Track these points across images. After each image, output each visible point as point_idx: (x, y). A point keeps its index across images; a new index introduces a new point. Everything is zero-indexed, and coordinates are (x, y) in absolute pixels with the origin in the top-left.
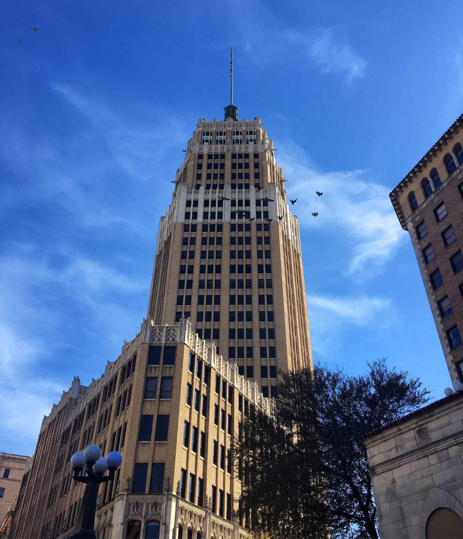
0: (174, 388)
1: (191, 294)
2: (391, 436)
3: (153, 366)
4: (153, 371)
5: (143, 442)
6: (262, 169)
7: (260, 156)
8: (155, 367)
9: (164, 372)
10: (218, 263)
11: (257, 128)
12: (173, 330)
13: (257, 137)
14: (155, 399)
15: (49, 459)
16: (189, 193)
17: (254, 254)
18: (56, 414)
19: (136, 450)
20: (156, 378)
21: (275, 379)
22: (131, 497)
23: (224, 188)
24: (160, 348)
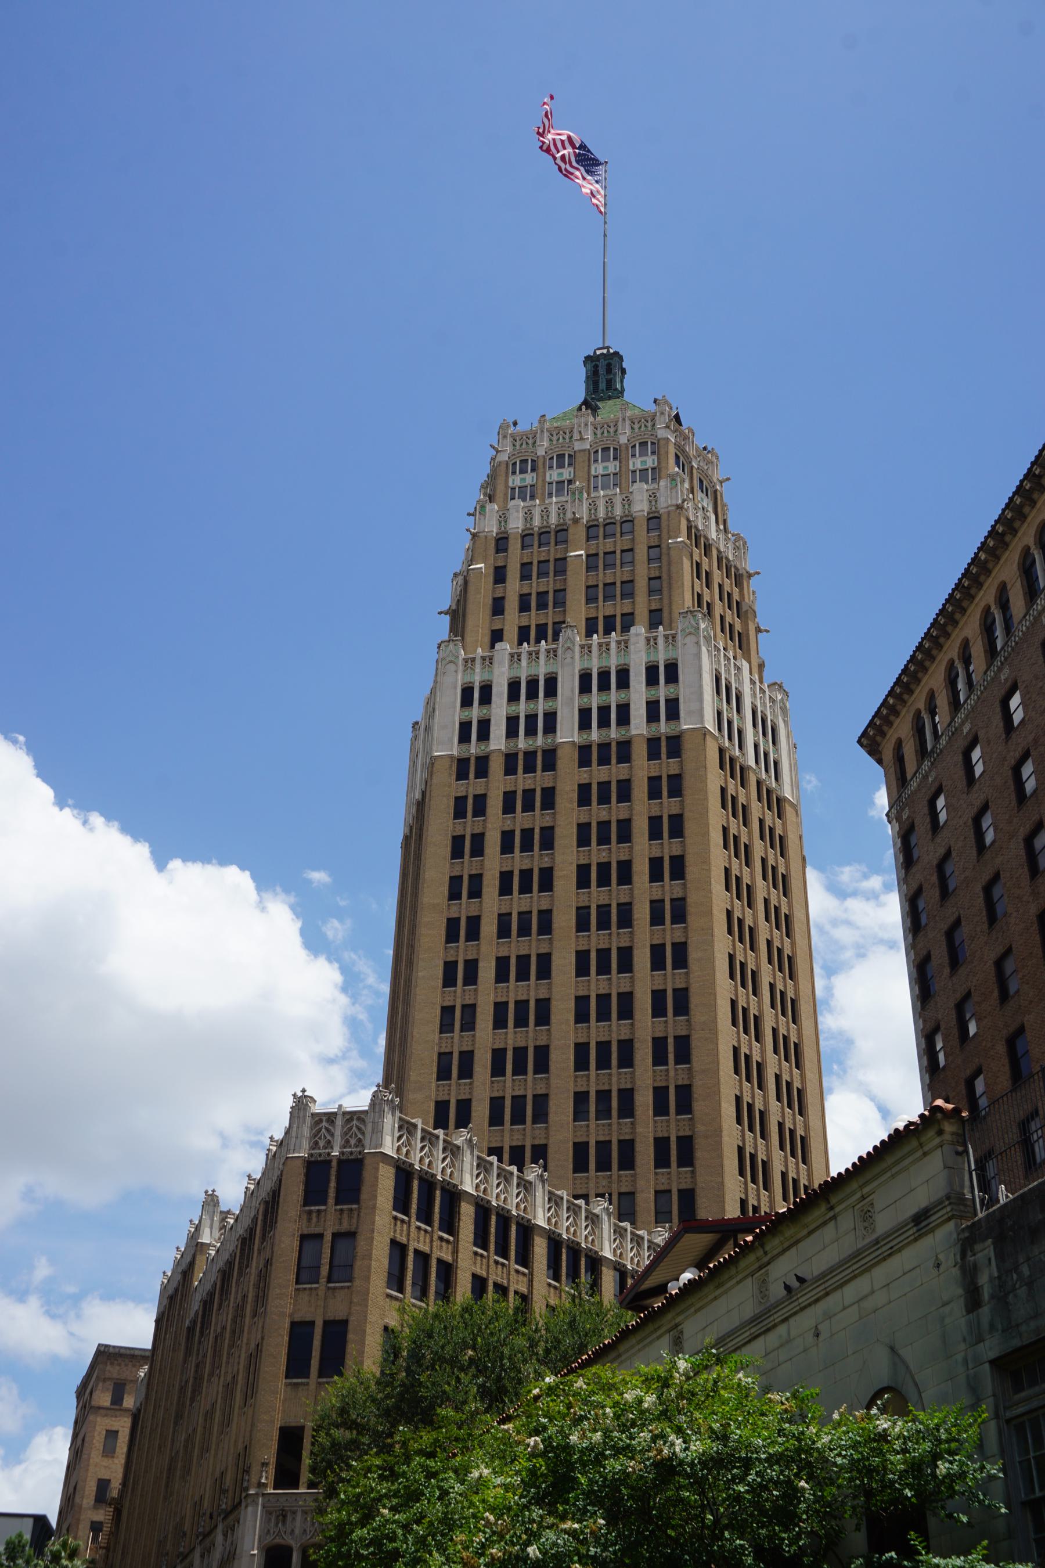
4: (314, 1219)
6: (669, 564)
8: (319, 1211)
20: (320, 1236)
24: (327, 1163)
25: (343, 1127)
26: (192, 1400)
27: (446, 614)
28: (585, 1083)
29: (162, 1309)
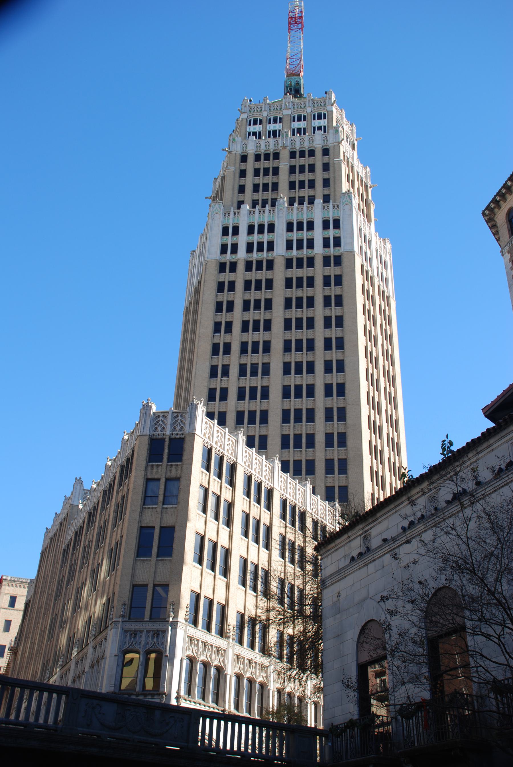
0: (182, 491)
1: (229, 361)
2: (342, 544)
3: (154, 464)
5: (142, 559)
6: (334, 172)
7: (331, 152)
8: (157, 466)
9: (168, 471)
10: (268, 317)
11: (329, 108)
12: (182, 416)
13: (328, 123)
14: (156, 506)
15: (50, 583)
16: (227, 214)
17: (319, 301)
18: (57, 526)
19: (133, 568)
21: (345, 475)
22: (128, 624)
23: (277, 204)
24: (163, 440)
25: (172, 420)
26: (68, 584)
27: (210, 199)
28: (288, 430)
29: (45, 546)
